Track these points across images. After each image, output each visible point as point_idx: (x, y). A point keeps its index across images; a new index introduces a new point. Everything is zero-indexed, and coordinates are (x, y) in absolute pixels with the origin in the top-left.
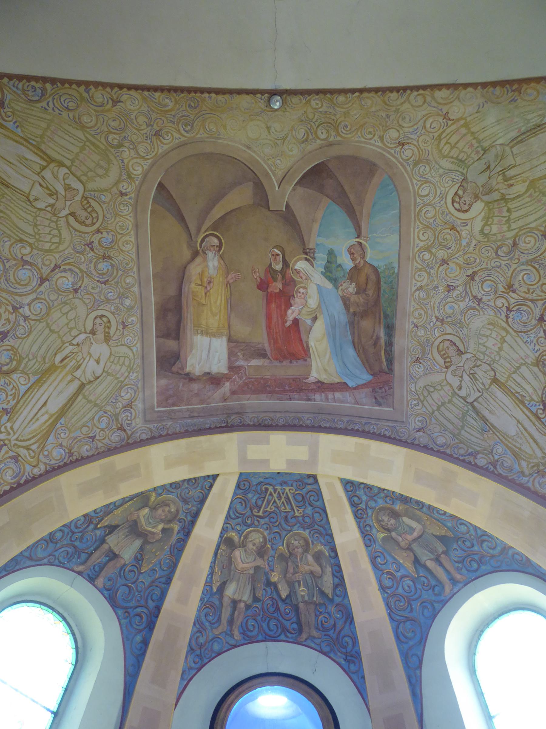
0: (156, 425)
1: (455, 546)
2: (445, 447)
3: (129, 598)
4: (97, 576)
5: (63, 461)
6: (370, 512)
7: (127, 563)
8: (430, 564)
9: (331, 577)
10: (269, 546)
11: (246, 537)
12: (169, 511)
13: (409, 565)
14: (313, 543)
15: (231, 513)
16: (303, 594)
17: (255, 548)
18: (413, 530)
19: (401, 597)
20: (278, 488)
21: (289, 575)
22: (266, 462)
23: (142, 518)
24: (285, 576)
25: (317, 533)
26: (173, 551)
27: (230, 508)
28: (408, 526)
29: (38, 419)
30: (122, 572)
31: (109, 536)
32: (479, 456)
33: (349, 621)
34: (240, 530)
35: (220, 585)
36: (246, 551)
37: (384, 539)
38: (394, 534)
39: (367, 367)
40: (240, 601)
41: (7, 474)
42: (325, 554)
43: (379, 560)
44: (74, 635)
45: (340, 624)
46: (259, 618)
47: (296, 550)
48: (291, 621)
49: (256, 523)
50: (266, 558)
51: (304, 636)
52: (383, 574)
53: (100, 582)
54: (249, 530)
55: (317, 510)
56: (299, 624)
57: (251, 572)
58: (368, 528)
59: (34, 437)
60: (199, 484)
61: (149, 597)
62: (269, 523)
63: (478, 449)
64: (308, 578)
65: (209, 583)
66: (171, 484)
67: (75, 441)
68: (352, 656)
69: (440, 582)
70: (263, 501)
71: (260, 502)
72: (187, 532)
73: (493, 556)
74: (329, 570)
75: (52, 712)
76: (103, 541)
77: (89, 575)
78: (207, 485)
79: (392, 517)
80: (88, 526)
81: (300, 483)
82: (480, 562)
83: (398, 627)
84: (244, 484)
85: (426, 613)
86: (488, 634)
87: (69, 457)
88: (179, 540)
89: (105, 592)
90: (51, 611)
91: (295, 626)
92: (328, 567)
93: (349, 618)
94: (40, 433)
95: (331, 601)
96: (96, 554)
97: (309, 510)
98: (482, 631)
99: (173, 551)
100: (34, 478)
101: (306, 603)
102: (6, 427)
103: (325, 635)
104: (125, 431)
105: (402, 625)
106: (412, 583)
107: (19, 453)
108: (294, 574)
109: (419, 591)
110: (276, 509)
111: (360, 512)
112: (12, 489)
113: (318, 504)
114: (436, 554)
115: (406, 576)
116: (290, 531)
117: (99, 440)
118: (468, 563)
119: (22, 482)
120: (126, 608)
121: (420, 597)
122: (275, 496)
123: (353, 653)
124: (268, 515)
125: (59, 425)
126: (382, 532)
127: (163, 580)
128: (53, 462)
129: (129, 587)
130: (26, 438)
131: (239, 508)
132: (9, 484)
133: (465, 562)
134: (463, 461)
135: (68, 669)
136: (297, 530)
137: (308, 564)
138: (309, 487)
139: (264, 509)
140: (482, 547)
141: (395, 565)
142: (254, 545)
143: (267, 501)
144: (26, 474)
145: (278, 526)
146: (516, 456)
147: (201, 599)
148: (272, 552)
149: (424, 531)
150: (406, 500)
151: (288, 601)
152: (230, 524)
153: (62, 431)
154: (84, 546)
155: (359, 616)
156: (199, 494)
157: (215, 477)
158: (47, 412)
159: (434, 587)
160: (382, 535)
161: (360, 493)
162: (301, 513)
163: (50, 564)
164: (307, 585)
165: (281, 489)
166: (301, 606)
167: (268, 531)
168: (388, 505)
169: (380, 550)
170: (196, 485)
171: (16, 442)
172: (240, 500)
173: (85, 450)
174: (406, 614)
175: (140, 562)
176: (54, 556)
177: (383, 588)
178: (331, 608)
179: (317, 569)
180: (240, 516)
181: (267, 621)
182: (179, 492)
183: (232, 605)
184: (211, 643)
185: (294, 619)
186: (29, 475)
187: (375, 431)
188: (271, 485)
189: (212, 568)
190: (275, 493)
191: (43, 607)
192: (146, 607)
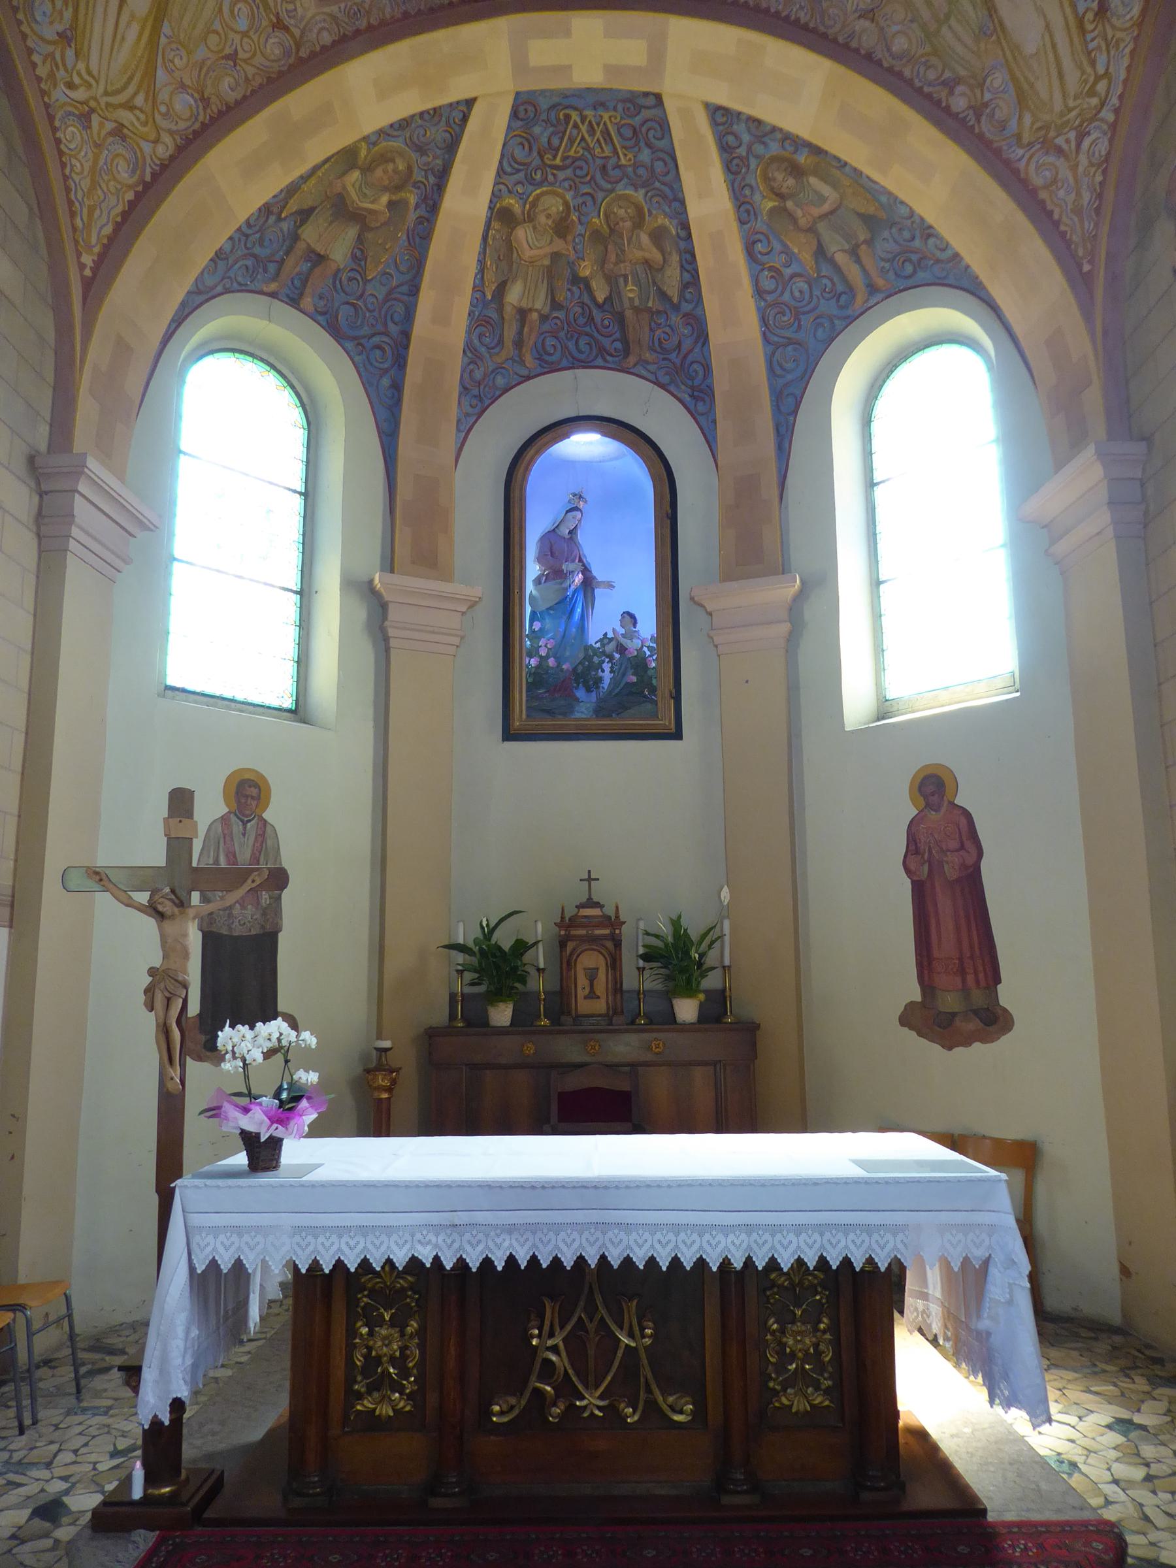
0: (343, 5)
1: (886, 234)
2: (904, 60)
3: (359, 323)
4: (301, 294)
5: (196, 119)
6: (753, 163)
7: (342, 267)
8: (841, 258)
9: (678, 271)
10: (574, 218)
11: (534, 204)
12: (395, 171)
13: (807, 258)
14: (650, 213)
15: (505, 164)
16: (631, 295)
17: (550, 222)
18: (822, 199)
19: (786, 308)
20: (589, 113)
21: (609, 266)
22: (566, 69)
23: (350, 188)
24: (602, 267)
25: (658, 195)
26: (413, 239)
27: (502, 156)
28: (816, 192)
29: (123, 38)
30: (338, 282)
31: (304, 227)
32: (960, 89)
33: (702, 340)
34: (523, 194)
35: (497, 287)
36: (534, 228)
37: (772, 211)
38: (789, 204)
39: (618, 963)
40: (530, 310)
41: (119, 168)
42: (669, 232)
43: (759, 247)
44: (293, 387)
45: (687, 344)
46: (562, 335)
47: (621, 224)
48: (612, 339)
49: (550, 178)
50: (570, 238)
51: (632, 359)
52: (763, 270)
53: (307, 302)
54: (538, 191)
55: (661, 155)
56: (625, 341)
57: (547, 262)
58: (747, 192)
59: (131, 78)
60: (441, 115)
61: (389, 318)
62: (573, 177)
63: (963, 73)
64: (640, 269)
65: (478, 288)
66: (392, 126)
67: (204, 71)
68: (701, 391)
69: (851, 290)
70: (562, 139)
71: (555, 141)
72: (432, 204)
73: (938, 261)
74: (675, 258)
75: (300, 493)
76: (296, 238)
77: (288, 296)
78: (457, 115)
79: (791, 174)
80: (267, 218)
81: (629, 105)
82: (918, 265)
83: (773, 354)
84: (526, 110)
85: (820, 333)
86: (881, 407)
87: (205, 109)
88: (420, 220)
89: (320, 318)
90: (251, 359)
91: (618, 345)
92: (674, 253)
93: (702, 337)
94: (137, 67)
95: (676, 308)
96: (290, 262)
97: (645, 155)
98: (896, 366)
99: (413, 239)
100: (164, 167)
101: (637, 310)
102: (79, 74)
103: (664, 359)
104: (286, 29)
105: (779, 350)
106: (806, 286)
107: (120, 121)
108: (616, 264)
109: (815, 300)
110: (586, 153)
111: (735, 162)
112: (139, 196)
113: (660, 144)
114: (854, 243)
115: (800, 275)
116: (612, 191)
117: (245, 61)
118: (901, 262)
119: (148, 178)
120: (354, 338)
121: (814, 309)
122: (584, 128)
123: (703, 387)
124: (571, 163)
125: (163, 40)
126: (771, 200)
127: (405, 289)
128: (182, 125)
129: (353, 304)
130: (118, 86)
131: (519, 154)
132: (130, 187)
133: (895, 262)
134: (929, 96)
135: (301, 436)
136: (623, 190)
137: (640, 248)
138: (646, 113)
139: (564, 152)
140: (926, 243)
141: (783, 256)
142: (548, 216)
143: (569, 138)
144: (148, 161)
145: (589, 182)
146: (1021, 100)
147: (469, 314)
148: (580, 229)
149: (841, 204)
150: (817, 151)
151: (606, 307)
152: (503, 183)
153: (173, 53)
154: (268, 251)
155: (717, 335)
156: (444, 134)
157: (470, 103)
158: (133, 16)
159: (840, 295)
160: (770, 204)
161: (740, 128)
162: (630, 160)
163: (227, 291)
164: (637, 282)
165: (595, 116)
166: (629, 314)
167: (572, 193)
168: (787, 154)
169: (764, 229)
170: (436, 119)
171: (105, 99)
172: (519, 140)
173: (227, 88)
174: (788, 334)
175: (363, 263)
176: (229, 278)
177: (759, 292)
178: (675, 319)
179: (656, 256)
180: (521, 167)
181: (575, 339)
182: (408, 136)
183: (518, 317)
184: (492, 376)
185: (618, 335)
186: (154, 162)
187: (780, 7)
188: (576, 109)
189: (481, 263)
190: (583, 123)
191: (237, 355)
192: (386, 333)
